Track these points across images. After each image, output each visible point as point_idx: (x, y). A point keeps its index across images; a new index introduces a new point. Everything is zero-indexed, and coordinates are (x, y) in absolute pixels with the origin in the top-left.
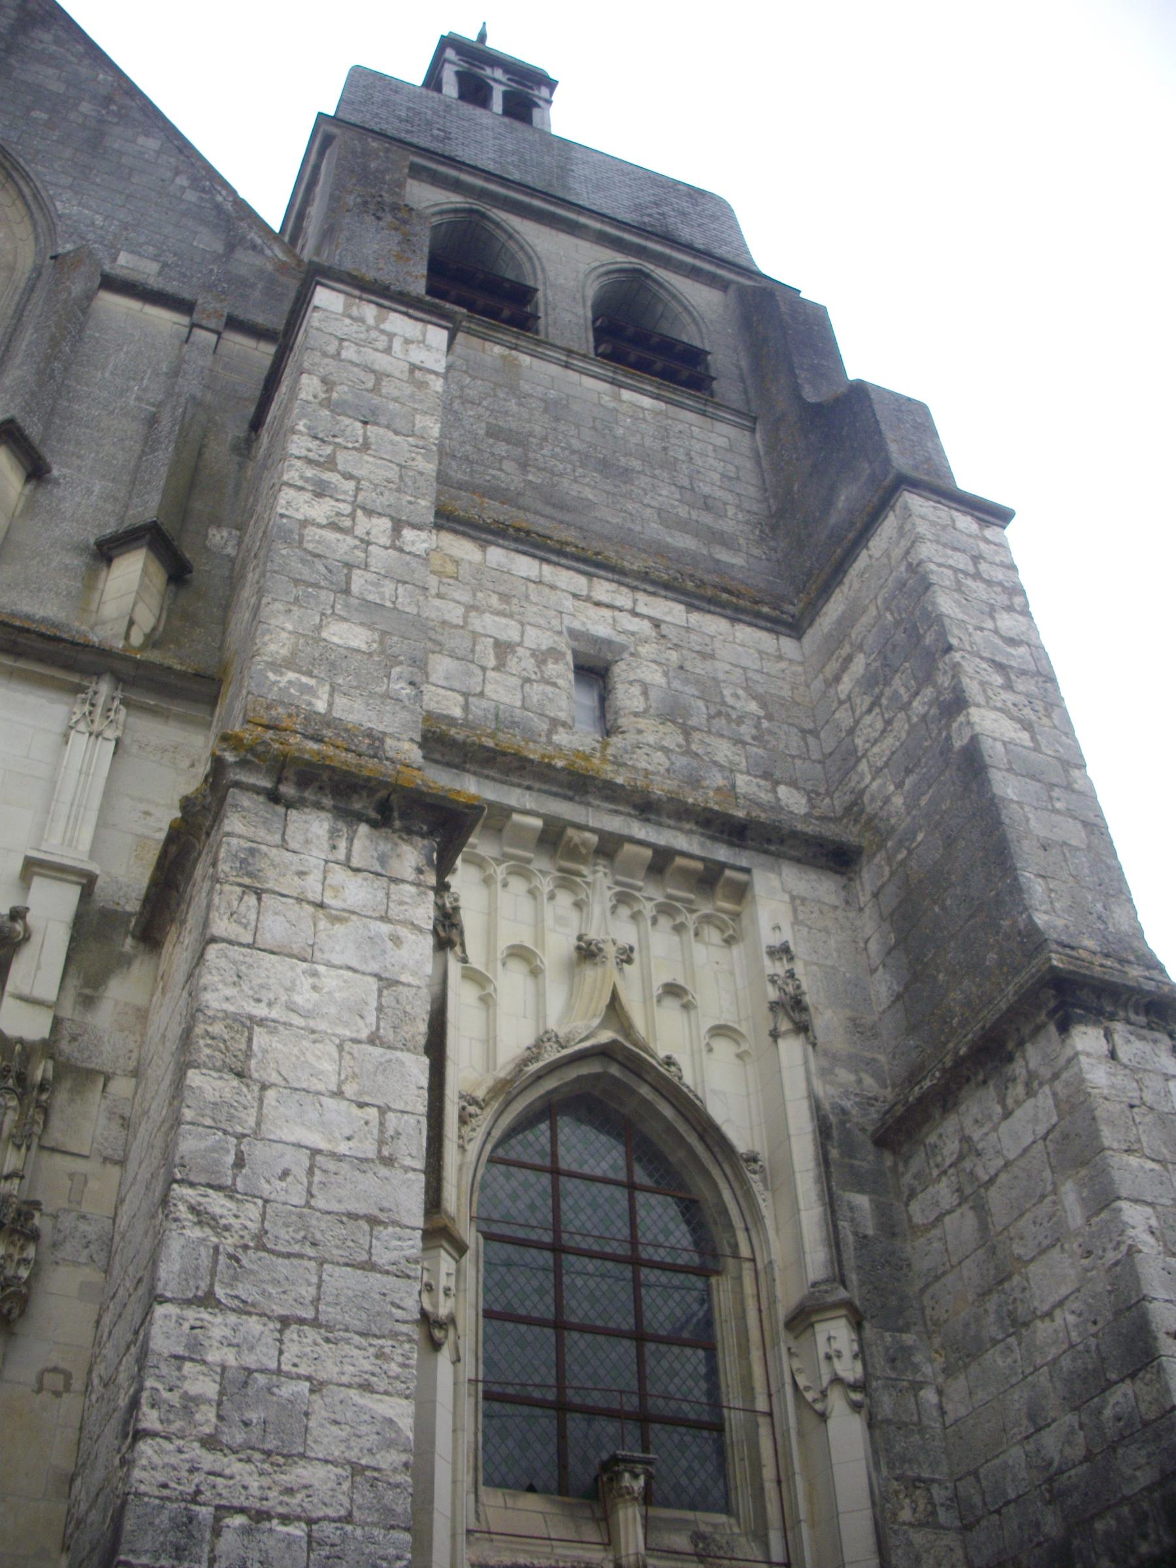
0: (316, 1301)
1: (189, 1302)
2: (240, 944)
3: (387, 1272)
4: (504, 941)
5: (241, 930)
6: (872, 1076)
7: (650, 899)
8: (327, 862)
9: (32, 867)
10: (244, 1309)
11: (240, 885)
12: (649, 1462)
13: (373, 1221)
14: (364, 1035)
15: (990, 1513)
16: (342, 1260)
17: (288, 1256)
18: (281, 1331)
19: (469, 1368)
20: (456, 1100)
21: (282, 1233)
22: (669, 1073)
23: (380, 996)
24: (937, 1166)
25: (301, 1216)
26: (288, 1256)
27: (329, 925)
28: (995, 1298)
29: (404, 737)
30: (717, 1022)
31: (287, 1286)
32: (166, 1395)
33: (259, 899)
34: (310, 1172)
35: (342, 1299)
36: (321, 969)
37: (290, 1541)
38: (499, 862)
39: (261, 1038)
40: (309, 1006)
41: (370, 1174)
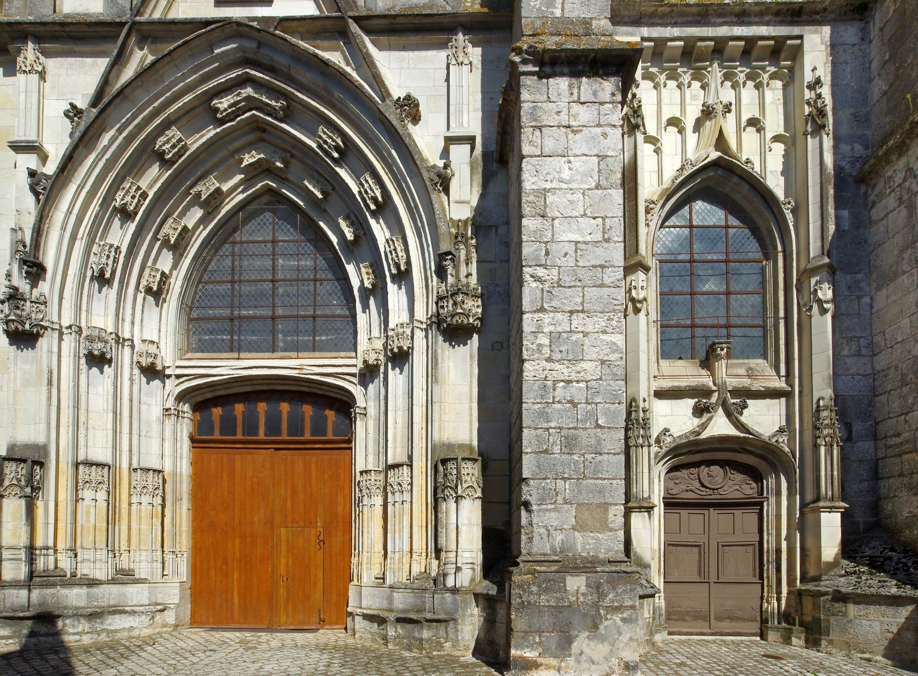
0: (582, 303)
1: (535, 312)
2: (536, 156)
3: (610, 287)
4: (665, 117)
5: (535, 149)
6: (861, 144)
7: (742, 72)
8: (569, 103)
9: (450, 140)
10: (556, 310)
11: (532, 127)
12: (729, 343)
13: (603, 267)
14: (593, 185)
15: (888, 348)
16: (591, 285)
17: (570, 287)
18: (570, 316)
19: (653, 316)
20: (644, 203)
21: (567, 279)
22: (748, 168)
23: (599, 165)
24: (890, 187)
25: (574, 271)
26: (570, 287)
27: (573, 136)
28: (909, 251)
29: (602, 17)
30: (775, 134)
31: (571, 299)
32: (531, 346)
33: (541, 132)
34: (576, 252)
35: (593, 300)
36: (572, 159)
37: (580, 389)
38: (661, 73)
39: (550, 198)
40: (568, 178)
41: (600, 248)
